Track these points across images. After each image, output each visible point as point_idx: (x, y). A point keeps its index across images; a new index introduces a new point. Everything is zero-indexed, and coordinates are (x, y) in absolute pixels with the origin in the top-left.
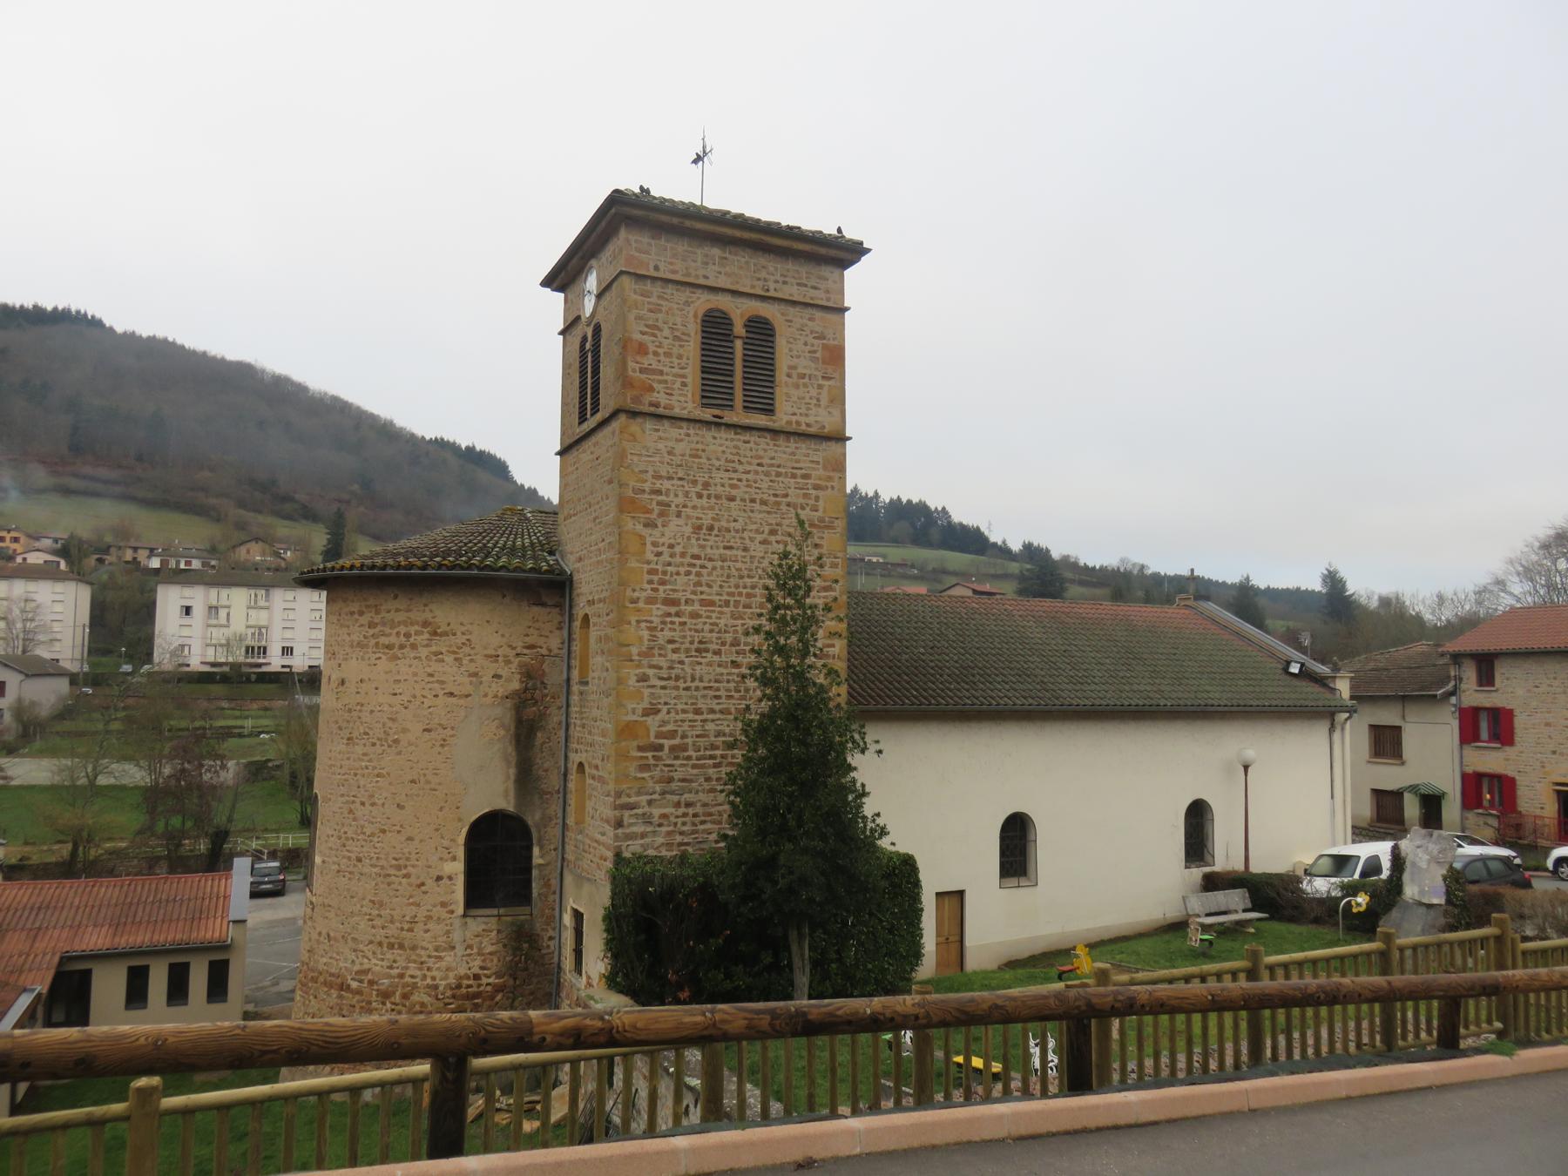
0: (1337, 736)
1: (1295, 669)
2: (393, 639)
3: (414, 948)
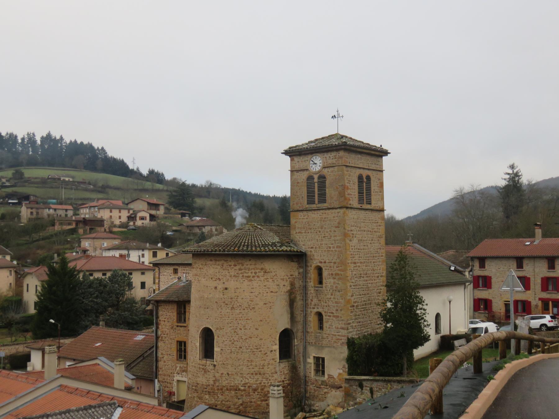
1: (453, 268)
2: (250, 274)
3: (264, 374)
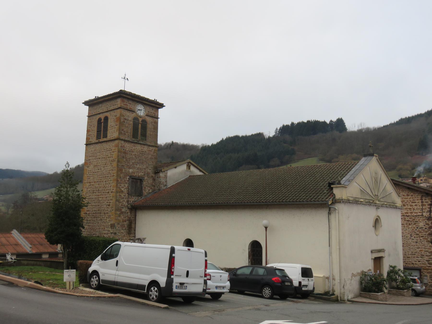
0: (332, 216)
